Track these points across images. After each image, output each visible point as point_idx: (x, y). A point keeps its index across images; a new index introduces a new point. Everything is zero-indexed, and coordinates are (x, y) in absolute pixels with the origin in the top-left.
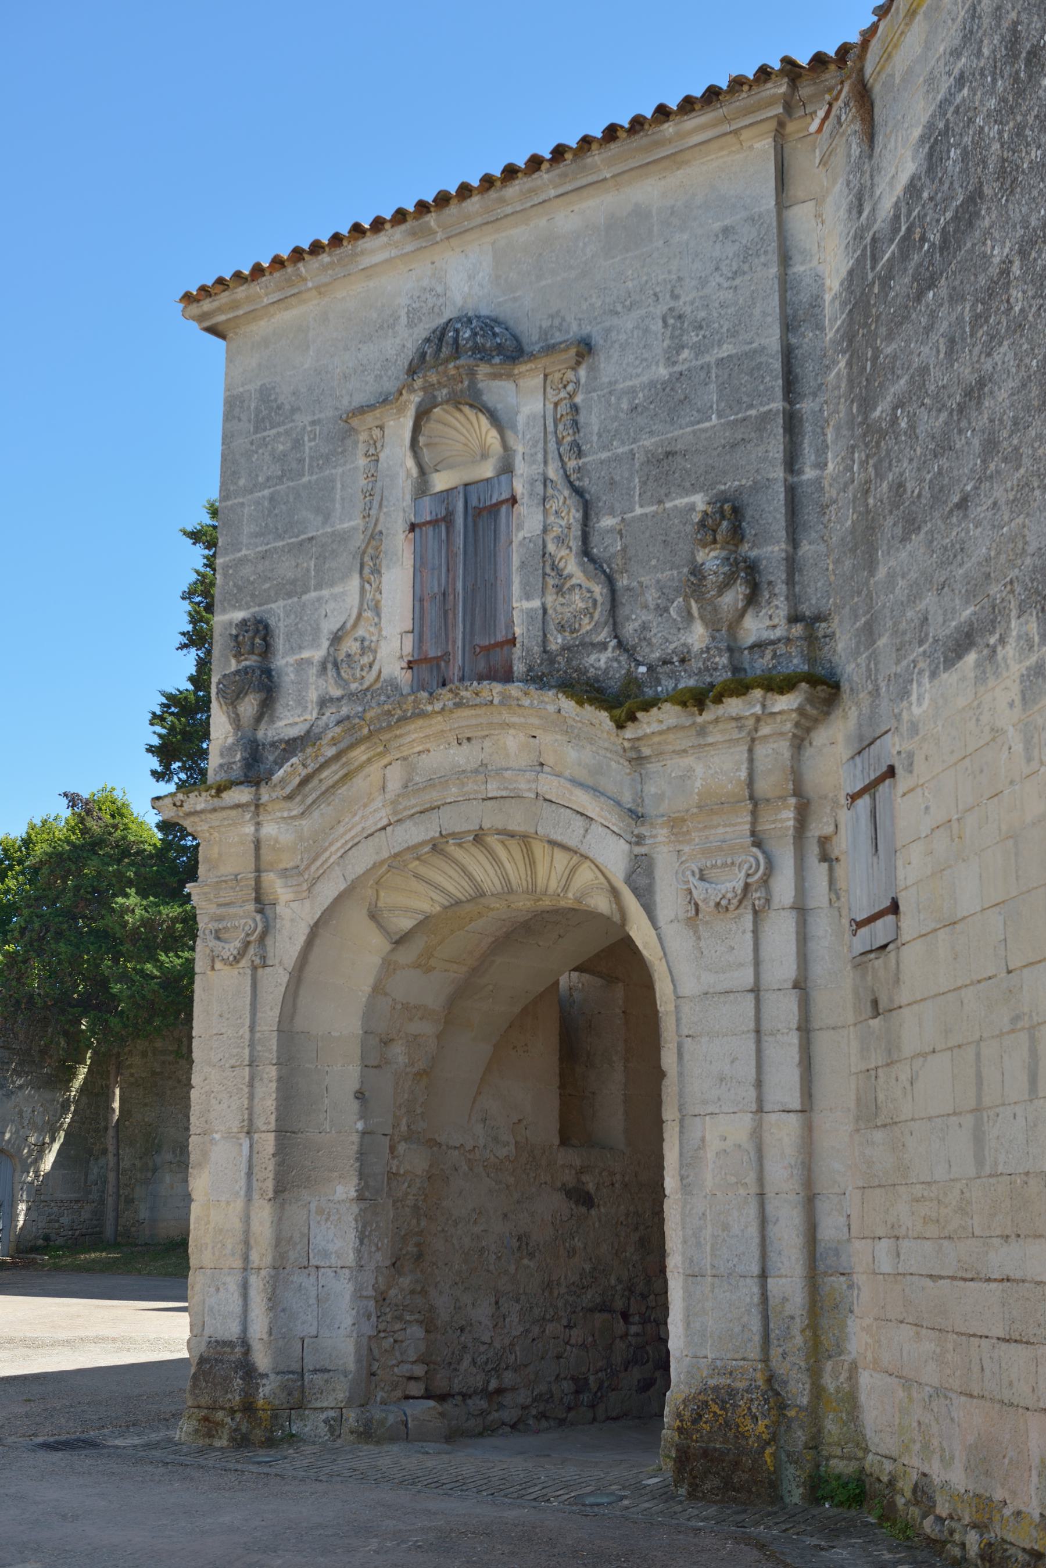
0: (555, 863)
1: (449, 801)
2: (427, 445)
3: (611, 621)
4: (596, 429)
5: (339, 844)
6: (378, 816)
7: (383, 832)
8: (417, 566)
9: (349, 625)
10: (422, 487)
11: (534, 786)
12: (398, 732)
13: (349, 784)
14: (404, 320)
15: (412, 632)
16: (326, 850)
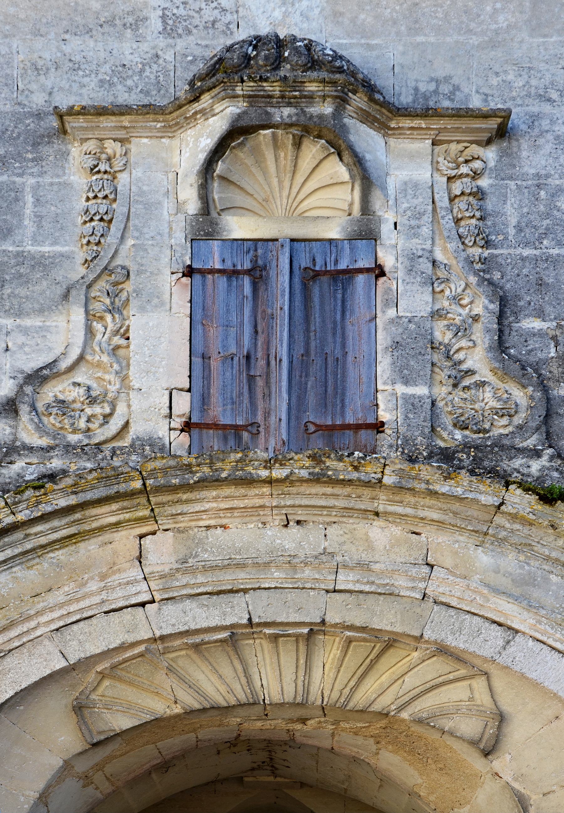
0: (407, 678)
1: (263, 586)
2: (222, 178)
3: (544, 429)
4: (513, 221)
5: (56, 614)
6: (133, 589)
7: (140, 609)
8: (198, 317)
9: (64, 365)
10: (205, 225)
11: (422, 585)
12: (184, 497)
13: (73, 548)
14: (156, 24)
15: (189, 390)
16: (29, 618)
